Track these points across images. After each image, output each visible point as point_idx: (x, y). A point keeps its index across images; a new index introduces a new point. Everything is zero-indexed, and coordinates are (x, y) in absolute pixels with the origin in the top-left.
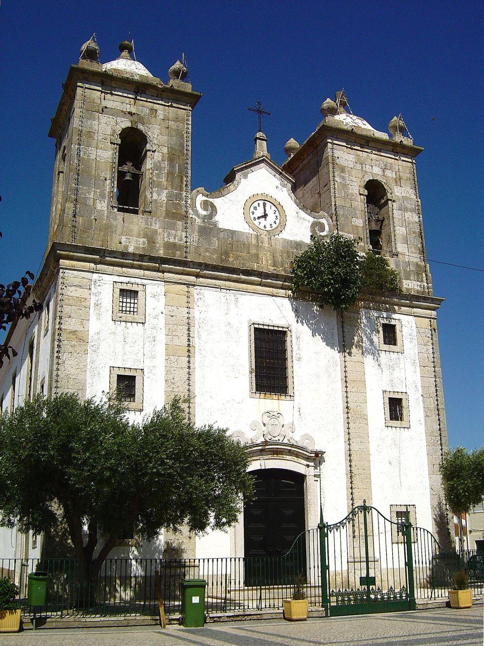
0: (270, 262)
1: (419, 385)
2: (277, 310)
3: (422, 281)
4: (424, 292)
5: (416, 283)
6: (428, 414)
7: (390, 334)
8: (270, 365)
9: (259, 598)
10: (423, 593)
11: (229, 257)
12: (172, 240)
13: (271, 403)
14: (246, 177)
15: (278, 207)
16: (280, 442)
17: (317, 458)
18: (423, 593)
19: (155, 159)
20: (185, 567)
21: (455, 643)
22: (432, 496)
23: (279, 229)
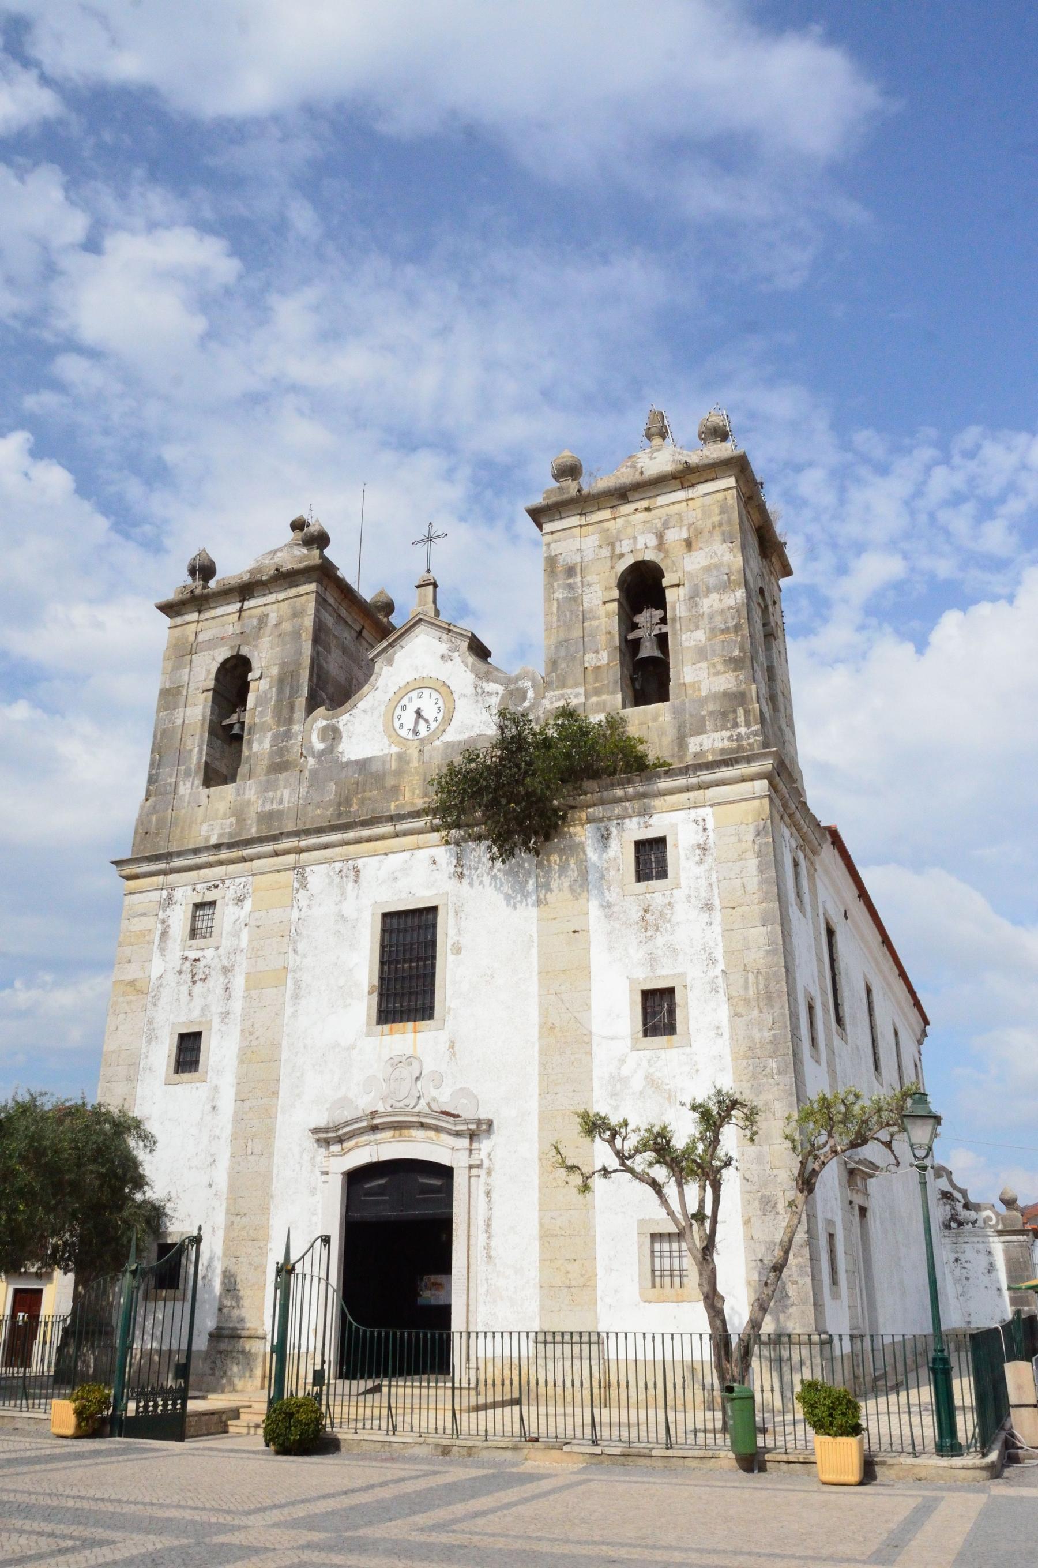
0: (417, 791)
1: (719, 954)
2: (415, 869)
3: (736, 725)
4: (740, 748)
5: (717, 735)
6: (740, 1010)
7: (651, 858)
8: (407, 971)
9: (457, 1392)
10: (570, 1427)
11: (351, 806)
12: (268, 808)
13: (407, 1038)
14: (390, 662)
15: (443, 689)
16: (408, 1109)
17: (477, 1131)
18: (570, 1427)
19: (260, 688)
20: (240, 1337)
21: (337, 1559)
22: (747, 1195)
23: (441, 728)
